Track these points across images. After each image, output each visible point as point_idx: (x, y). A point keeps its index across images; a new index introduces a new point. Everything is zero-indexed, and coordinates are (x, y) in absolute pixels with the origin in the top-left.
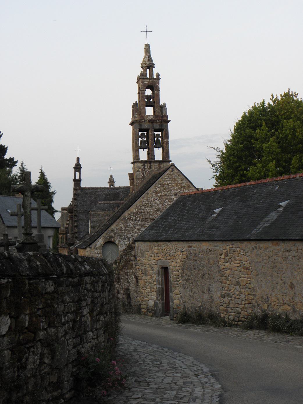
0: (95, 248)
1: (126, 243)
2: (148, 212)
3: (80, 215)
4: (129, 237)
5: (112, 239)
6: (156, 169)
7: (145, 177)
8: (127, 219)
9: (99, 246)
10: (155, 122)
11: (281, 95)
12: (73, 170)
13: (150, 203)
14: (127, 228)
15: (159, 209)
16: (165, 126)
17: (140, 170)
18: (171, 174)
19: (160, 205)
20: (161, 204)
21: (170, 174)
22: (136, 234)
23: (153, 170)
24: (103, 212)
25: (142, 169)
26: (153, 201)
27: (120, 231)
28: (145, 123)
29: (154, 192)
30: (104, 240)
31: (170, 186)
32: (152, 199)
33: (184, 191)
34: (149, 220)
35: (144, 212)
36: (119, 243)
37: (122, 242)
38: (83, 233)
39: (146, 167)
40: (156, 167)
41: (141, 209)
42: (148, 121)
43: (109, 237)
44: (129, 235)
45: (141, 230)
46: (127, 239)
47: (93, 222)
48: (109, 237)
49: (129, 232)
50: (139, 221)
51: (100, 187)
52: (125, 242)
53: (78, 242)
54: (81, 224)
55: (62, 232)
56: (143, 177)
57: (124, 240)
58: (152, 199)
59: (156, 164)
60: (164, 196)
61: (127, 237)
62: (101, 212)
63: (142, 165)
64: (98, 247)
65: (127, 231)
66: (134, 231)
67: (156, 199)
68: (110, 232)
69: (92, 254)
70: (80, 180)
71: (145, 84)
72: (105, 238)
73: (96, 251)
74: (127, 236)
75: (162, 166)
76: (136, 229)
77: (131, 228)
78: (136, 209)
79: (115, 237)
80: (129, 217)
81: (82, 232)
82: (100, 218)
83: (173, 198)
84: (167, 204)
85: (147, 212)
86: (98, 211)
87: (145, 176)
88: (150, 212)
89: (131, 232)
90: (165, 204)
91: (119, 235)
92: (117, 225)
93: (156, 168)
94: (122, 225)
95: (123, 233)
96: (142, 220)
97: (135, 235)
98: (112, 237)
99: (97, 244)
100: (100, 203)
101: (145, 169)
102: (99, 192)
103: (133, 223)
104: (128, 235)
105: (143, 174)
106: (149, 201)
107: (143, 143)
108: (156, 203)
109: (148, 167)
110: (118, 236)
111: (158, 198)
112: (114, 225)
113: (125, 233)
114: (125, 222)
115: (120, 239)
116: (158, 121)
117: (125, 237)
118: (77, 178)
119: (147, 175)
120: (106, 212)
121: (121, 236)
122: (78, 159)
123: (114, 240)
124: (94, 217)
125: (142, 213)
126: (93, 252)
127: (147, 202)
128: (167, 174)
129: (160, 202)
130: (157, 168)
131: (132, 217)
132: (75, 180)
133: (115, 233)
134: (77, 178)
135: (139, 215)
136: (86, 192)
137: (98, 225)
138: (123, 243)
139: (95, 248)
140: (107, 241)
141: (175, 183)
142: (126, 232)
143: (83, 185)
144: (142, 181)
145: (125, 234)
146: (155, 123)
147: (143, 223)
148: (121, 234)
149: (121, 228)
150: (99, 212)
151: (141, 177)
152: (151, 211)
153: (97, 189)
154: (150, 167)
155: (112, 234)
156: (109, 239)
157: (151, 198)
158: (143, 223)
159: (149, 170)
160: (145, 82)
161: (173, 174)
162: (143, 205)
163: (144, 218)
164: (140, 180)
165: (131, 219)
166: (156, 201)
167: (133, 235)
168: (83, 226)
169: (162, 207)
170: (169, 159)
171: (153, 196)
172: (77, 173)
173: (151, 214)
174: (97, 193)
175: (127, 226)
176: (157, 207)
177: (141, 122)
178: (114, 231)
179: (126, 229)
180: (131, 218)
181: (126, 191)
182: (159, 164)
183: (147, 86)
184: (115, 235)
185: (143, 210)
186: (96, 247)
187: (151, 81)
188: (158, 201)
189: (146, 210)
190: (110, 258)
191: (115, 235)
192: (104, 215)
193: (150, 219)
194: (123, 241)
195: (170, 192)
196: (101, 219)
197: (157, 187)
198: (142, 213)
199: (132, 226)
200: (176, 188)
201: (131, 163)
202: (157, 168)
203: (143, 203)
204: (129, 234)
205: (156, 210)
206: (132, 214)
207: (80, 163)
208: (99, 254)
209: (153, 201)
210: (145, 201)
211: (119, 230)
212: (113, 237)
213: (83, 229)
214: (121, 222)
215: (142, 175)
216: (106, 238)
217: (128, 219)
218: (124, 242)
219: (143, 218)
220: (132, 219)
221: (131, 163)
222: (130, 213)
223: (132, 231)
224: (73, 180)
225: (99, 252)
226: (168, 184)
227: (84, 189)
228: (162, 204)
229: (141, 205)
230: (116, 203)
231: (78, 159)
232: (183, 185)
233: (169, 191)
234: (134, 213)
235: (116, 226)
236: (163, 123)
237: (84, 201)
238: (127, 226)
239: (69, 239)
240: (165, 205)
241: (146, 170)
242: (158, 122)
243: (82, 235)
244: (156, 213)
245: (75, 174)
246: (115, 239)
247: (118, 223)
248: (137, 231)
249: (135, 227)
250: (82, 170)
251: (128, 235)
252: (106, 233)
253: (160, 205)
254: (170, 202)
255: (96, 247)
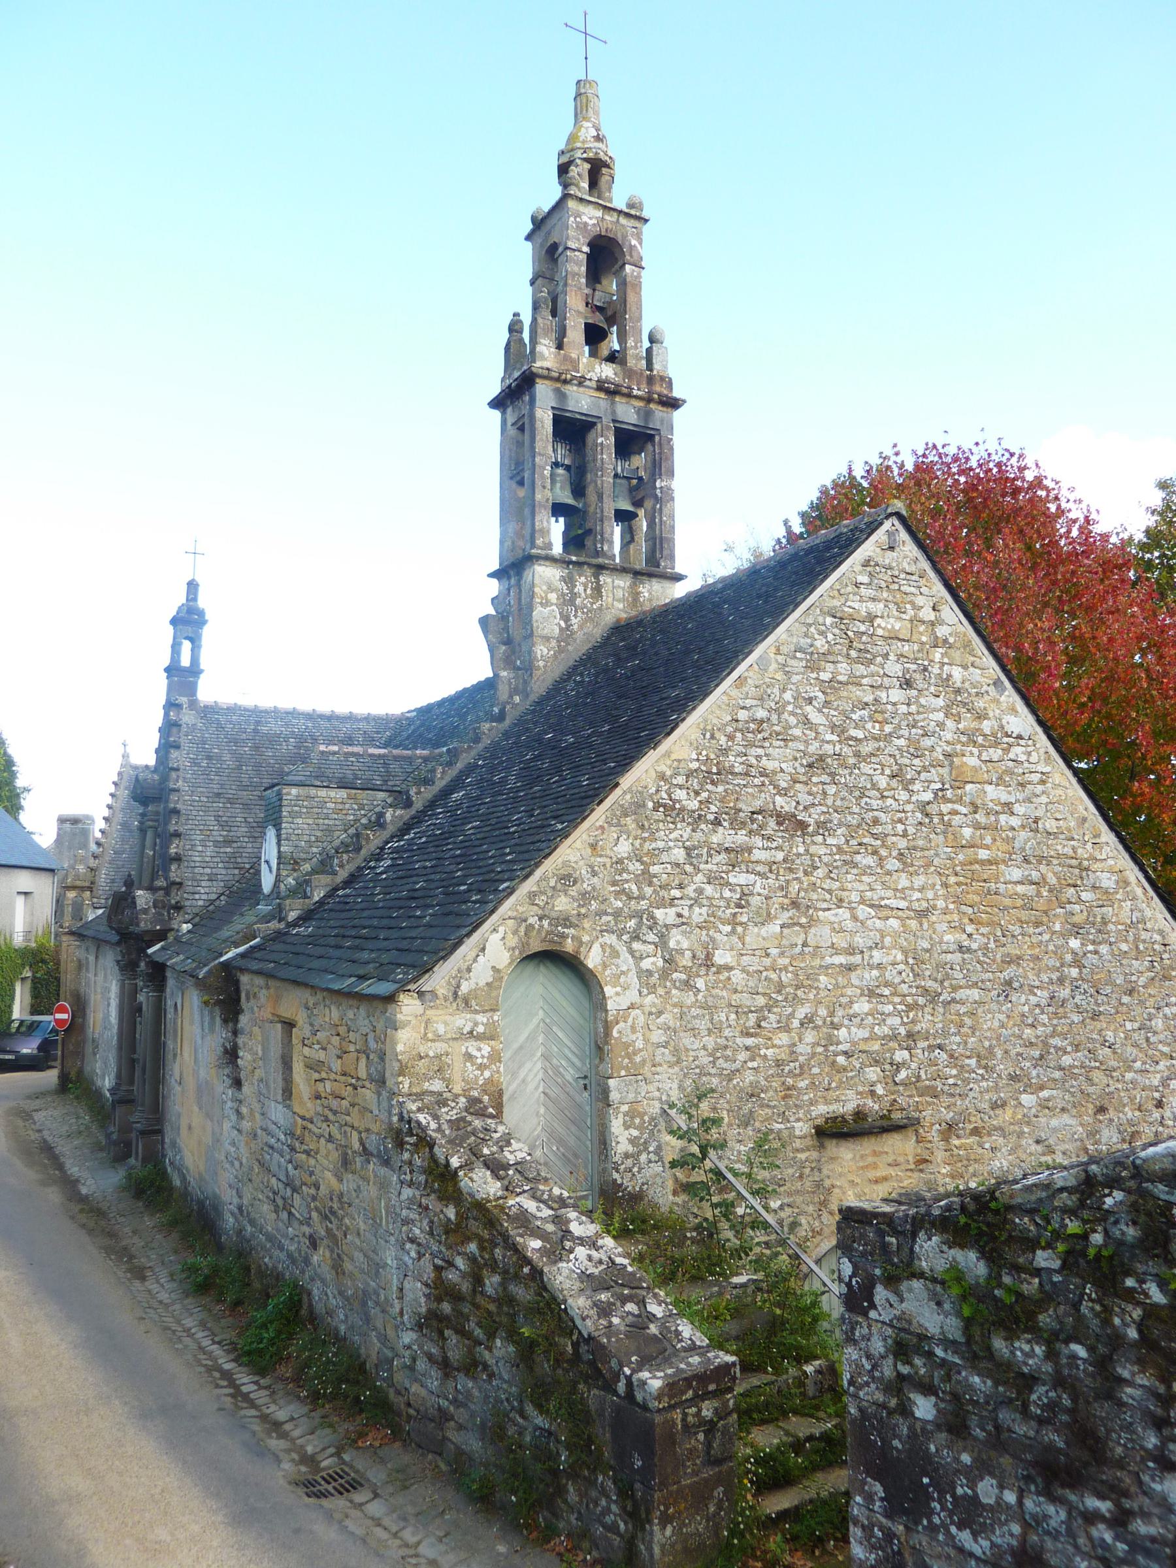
0: (455, 994)
1: (646, 964)
2: (767, 776)
3: (194, 813)
4: (666, 926)
5: (563, 936)
6: (621, 606)
7: (573, 633)
8: (650, 805)
9: (482, 983)
10: (624, 395)
11: (914, 452)
12: (170, 629)
13: (774, 718)
14: (654, 869)
15: (821, 758)
16: (662, 421)
17: (553, 597)
18: (887, 562)
19: (829, 737)
20: (833, 728)
21: (880, 560)
22: (701, 906)
23: (608, 608)
24: (343, 794)
25: (563, 595)
26: (790, 708)
27: (614, 883)
28: (581, 389)
29: (798, 655)
30: (513, 941)
31: (880, 632)
32: (788, 696)
33: (946, 667)
34: (772, 823)
35: (747, 774)
36: (605, 966)
37: (625, 961)
38: (207, 890)
39: (579, 588)
40: (619, 593)
41: (725, 752)
42: (594, 384)
43: (546, 923)
44: (665, 915)
45: (728, 884)
46: (651, 937)
47: (294, 838)
48: (546, 923)
49: (662, 893)
50: (717, 822)
51: (276, 710)
52: (641, 958)
53: (185, 926)
54: (200, 848)
55: (78, 883)
56: (567, 633)
57: (636, 945)
58: (788, 696)
59: (622, 583)
60: (847, 684)
61: (654, 924)
62: (332, 793)
63: (563, 579)
64: (474, 992)
65: (650, 884)
66: (690, 891)
67: (810, 701)
68: (554, 888)
69: (438, 1038)
70: (195, 670)
71: (586, 224)
72: (522, 929)
73: (463, 1021)
74: (652, 917)
75: (646, 595)
76: (699, 878)
77: (678, 865)
78: (705, 748)
79: (587, 924)
80: (665, 796)
81: (203, 884)
82: (326, 822)
83: (894, 704)
84: (860, 734)
85: (763, 774)
86: (319, 783)
87: (575, 627)
88: (774, 772)
89: (676, 893)
90: (853, 732)
91: (606, 914)
92: (593, 846)
93: (619, 601)
94: (624, 848)
95: (630, 898)
96: (737, 824)
97: (697, 910)
98: (566, 921)
99: (469, 970)
100: (323, 752)
101: (575, 596)
102: (273, 727)
103: (686, 836)
104: (659, 913)
105: (566, 619)
106: (773, 704)
107: (558, 485)
108: (806, 722)
109: (589, 591)
110: (601, 913)
111: (820, 694)
112: (578, 844)
113: (641, 897)
114: (642, 827)
115: (611, 939)
116: (635, 392)
117: (640, 924)
118: (185, 661)
119: (581, 627)
120: (354, 791)
121: (617, 914)
122: (192, 586)
123: (581, 943)
124: (299, 815)
125: (732, 773)
126: (441, 1030)
127: (761, 714)
128: (866, 563)
129: (827, 716)
130: (623, 600)
131: (680, 794)
132: (173, 670)
133: (585, 897)
134: (185, 661)
135: (720, 789)
136: (217, 719)
137: (315, 850)
138: (631, 960)
139: (455, 994)
140: (536, 946)
141: (904, 616)
142: (648, 891)
143: (208, 692)
144: (561, 650)
145: (644, 904)
146: (624, 400)
147: (741, 837)
148: (619, 904)
149: (620, 861)
150: (322, 793)
151: (557, 631)
152: (784, 766)
153: (261, 712)
154: (598, 590)
155: (563, 904)
156: (548, 933)
157: (784, 690)
158: (741, 837)
159: (592, 604)
160: (585, 219)
161: (894, 564)
162: (740, 725)
163: (744, 807)
164: (554, 643)
165: (672, 811)
166: (809, 709)
167: (686, 913)
168: (208, 859)
169: (838, 747)
170: (673, 568)
171: (795, 678)
172: (186, 646)
173: (784, 784)
174: (264, 729)
175: (652, 853)
176: (812, 749)
177: (565, 382)
178: (575, 882)
179: (645, 872)
180: (674, 801)
181: (378, 733)
182: (634, 586)
183: (593, 234)
184: (583, 911)
185: (739, 760)
186: (465, 988)
187: (607, 217)
188: (820, 711)
189: (753, 761)
190: (539, 1065)
191: (583, 911)
192: (347, 806)
193: (779, 815)
194: (632, 952)
195: (882, 666)
196: (331, 823)
197: (812, 629)
198: (732, 773)
199: (679, 854)
200: (906, 648)
201: (491, 575)
202: (623, 600)
203: (743, 715)
204: (662, 904)
205: (810, 766)
206: (680, 780)
207: (202, 603)
208: (480, 1038)
209: (790, 708)
210: (748, 703)
211: (604, 874)
212: (574, 920)
213: (208, 871)
214: (618, 825)
215: (563, 624)
216: (531, 927)
217: (655, 809)
218: (638, 958)
219: (740, 805)
220: (682, 809)
221: (491, 575)
222: (668, 773)
223: (681, 886)
224: (167, 670)
225: (481, 1029)
226: (871, 618)
227: (212, 707)
228: (838, 729)
229: (729, 729)
230: (396, 758)
231: (192, 586)
232: (942, 631)
233: (875, 657)
234: (690, 774)
235: (589, 850)
236: (652, 406)
237: (209, 758)
238: (655, 854)
239: (145, 911)
240: (851, 738)
241: (578, 601)
242: (636, 397)
243: (204, 897)
244: (806, 783)
245: (176, 648)
246: (586, 938)
247: (602, 827)
248: (709, 890)
249: (695, 861)
250: (207, 633)
251: (659, 913)
252: (532, 896)
253: (829, 737)
254: (877, 725)
255: (465, 988)
